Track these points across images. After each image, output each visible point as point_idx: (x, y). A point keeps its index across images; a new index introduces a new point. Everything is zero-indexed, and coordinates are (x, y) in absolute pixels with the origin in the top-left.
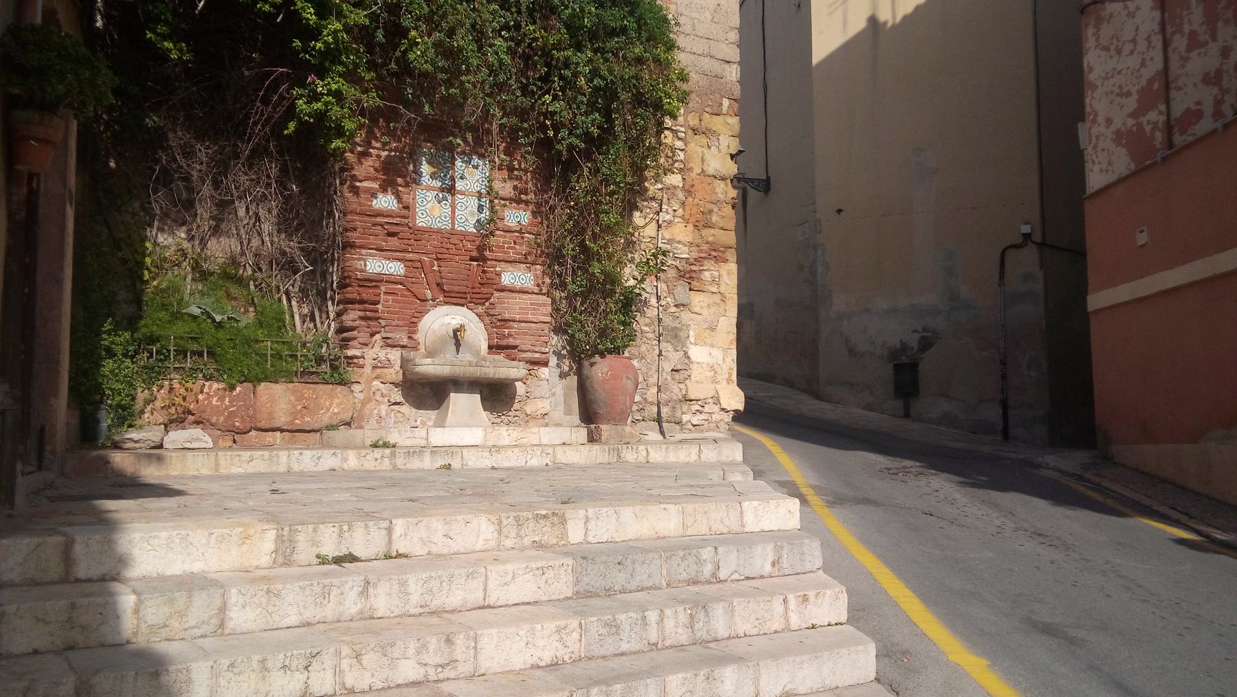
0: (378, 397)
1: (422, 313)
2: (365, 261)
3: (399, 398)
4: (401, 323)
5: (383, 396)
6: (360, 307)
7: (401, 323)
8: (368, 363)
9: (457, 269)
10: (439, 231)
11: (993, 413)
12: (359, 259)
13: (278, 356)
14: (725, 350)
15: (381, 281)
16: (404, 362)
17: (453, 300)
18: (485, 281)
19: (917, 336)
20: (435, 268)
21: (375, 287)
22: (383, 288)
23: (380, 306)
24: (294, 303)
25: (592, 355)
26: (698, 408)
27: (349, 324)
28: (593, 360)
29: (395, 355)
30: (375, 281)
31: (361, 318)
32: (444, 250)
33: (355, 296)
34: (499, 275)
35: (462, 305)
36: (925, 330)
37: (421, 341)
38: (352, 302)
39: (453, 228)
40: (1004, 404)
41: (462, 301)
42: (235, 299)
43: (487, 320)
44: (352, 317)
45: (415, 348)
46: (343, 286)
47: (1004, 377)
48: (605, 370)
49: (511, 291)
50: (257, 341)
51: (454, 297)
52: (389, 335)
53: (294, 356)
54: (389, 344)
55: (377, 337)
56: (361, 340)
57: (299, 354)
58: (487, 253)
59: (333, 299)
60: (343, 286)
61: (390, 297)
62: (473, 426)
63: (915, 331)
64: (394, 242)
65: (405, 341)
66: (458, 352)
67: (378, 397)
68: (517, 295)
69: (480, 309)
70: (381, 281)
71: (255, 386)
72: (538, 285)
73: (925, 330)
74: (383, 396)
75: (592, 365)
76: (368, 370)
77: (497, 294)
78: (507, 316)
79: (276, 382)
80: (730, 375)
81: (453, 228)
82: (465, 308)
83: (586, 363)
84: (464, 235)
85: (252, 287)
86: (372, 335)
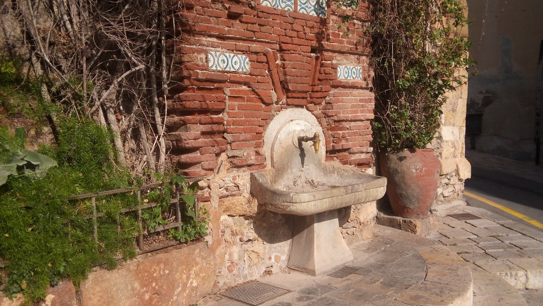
0: (227, 236)
1: (267, 120)
2: (206, 52)
3: (252, 234)
4: (248, 136)
5: (234, 234)
6: (202, 117)
7: (243, 136)
8: (216, 193)
9: (299, 62)
10: (282, 14)
11: (530, 147)
12: (199, 52)
13: (110, 220)
14: (460, 128)
15: (224, 82)
16: (258, 190)
17: (296, 101)
18: (322, 76)
19: (482, 96)
20: (278, 62)
21: (217, 89)
22: (227, 91)
23: (224, 116)
24: (112, 117)
25: (402, 149)
26: (446, 181)
27: (191, 143)
28: (401, 154)
29: (243, 179)
30: (216, 82)
31: (204, 134)
32: (289, 40)
33: (196, 104)
34: (334, 68)
35: (302, 106)
36: (487, 92)
37: (268, 154)
38: (191, 112)
39: (295, 11)
40: (537, 142)
41: (303, 102)
42: (19, 115)
43: (324, 121)
44: (192, 134)
45: (262, 166)
46: (176, 90)
47: (538, 124)
48: (419, 165)
49: (344, 87)
50: (74, 202)
51: (295, 98)
52: (236, 153)
53: (134, 215)
54: (236, 164)
55: (223, 156)
56: (206, 165)
57: (139, 209)
58: (325, 43)
59: (161, 107)
60: (176, 90)
61: (236, 103)
62: (351, 268)
63: (481, 93)
64: (238, 27)
65: (253, 159)
66: (303, 163)
67: (227, 236)
68: (347, 91)
69: (318, 111)
70: (224, 82)
71: (77, 285)
72: (365, 79)
73: (487, 92)
74: (234, 234)
75: (401, 159)
76: (215, 202)
77: (333, 91)
78: (342, 116)
79: (111, 266)
80: (462, 150)
81: (295, 11)
82: (304, 110)
83: (394, 157)
84: (305, 18)
85: (47, 97)
86: (218, 155)
